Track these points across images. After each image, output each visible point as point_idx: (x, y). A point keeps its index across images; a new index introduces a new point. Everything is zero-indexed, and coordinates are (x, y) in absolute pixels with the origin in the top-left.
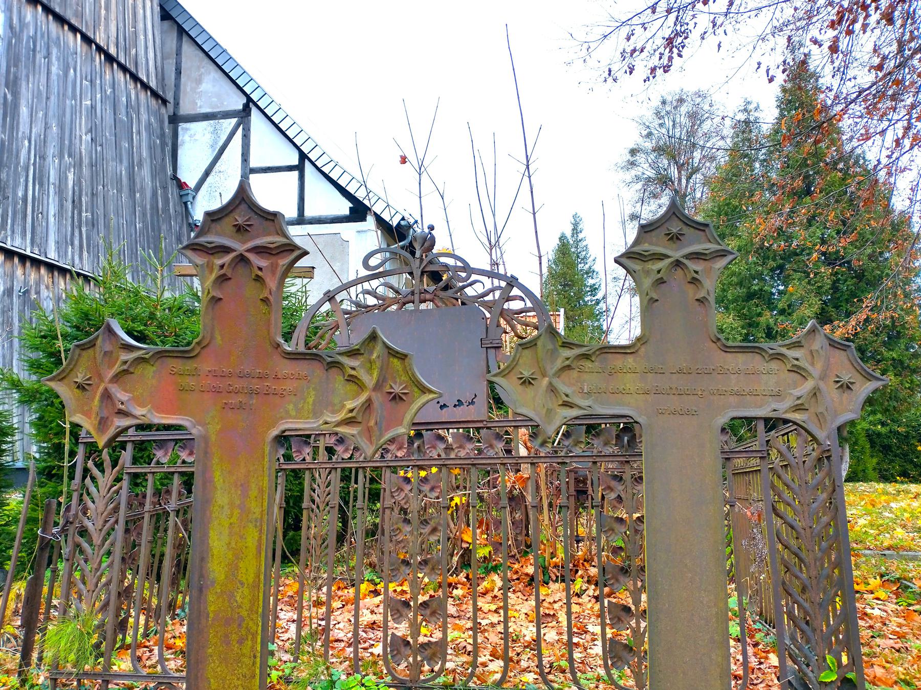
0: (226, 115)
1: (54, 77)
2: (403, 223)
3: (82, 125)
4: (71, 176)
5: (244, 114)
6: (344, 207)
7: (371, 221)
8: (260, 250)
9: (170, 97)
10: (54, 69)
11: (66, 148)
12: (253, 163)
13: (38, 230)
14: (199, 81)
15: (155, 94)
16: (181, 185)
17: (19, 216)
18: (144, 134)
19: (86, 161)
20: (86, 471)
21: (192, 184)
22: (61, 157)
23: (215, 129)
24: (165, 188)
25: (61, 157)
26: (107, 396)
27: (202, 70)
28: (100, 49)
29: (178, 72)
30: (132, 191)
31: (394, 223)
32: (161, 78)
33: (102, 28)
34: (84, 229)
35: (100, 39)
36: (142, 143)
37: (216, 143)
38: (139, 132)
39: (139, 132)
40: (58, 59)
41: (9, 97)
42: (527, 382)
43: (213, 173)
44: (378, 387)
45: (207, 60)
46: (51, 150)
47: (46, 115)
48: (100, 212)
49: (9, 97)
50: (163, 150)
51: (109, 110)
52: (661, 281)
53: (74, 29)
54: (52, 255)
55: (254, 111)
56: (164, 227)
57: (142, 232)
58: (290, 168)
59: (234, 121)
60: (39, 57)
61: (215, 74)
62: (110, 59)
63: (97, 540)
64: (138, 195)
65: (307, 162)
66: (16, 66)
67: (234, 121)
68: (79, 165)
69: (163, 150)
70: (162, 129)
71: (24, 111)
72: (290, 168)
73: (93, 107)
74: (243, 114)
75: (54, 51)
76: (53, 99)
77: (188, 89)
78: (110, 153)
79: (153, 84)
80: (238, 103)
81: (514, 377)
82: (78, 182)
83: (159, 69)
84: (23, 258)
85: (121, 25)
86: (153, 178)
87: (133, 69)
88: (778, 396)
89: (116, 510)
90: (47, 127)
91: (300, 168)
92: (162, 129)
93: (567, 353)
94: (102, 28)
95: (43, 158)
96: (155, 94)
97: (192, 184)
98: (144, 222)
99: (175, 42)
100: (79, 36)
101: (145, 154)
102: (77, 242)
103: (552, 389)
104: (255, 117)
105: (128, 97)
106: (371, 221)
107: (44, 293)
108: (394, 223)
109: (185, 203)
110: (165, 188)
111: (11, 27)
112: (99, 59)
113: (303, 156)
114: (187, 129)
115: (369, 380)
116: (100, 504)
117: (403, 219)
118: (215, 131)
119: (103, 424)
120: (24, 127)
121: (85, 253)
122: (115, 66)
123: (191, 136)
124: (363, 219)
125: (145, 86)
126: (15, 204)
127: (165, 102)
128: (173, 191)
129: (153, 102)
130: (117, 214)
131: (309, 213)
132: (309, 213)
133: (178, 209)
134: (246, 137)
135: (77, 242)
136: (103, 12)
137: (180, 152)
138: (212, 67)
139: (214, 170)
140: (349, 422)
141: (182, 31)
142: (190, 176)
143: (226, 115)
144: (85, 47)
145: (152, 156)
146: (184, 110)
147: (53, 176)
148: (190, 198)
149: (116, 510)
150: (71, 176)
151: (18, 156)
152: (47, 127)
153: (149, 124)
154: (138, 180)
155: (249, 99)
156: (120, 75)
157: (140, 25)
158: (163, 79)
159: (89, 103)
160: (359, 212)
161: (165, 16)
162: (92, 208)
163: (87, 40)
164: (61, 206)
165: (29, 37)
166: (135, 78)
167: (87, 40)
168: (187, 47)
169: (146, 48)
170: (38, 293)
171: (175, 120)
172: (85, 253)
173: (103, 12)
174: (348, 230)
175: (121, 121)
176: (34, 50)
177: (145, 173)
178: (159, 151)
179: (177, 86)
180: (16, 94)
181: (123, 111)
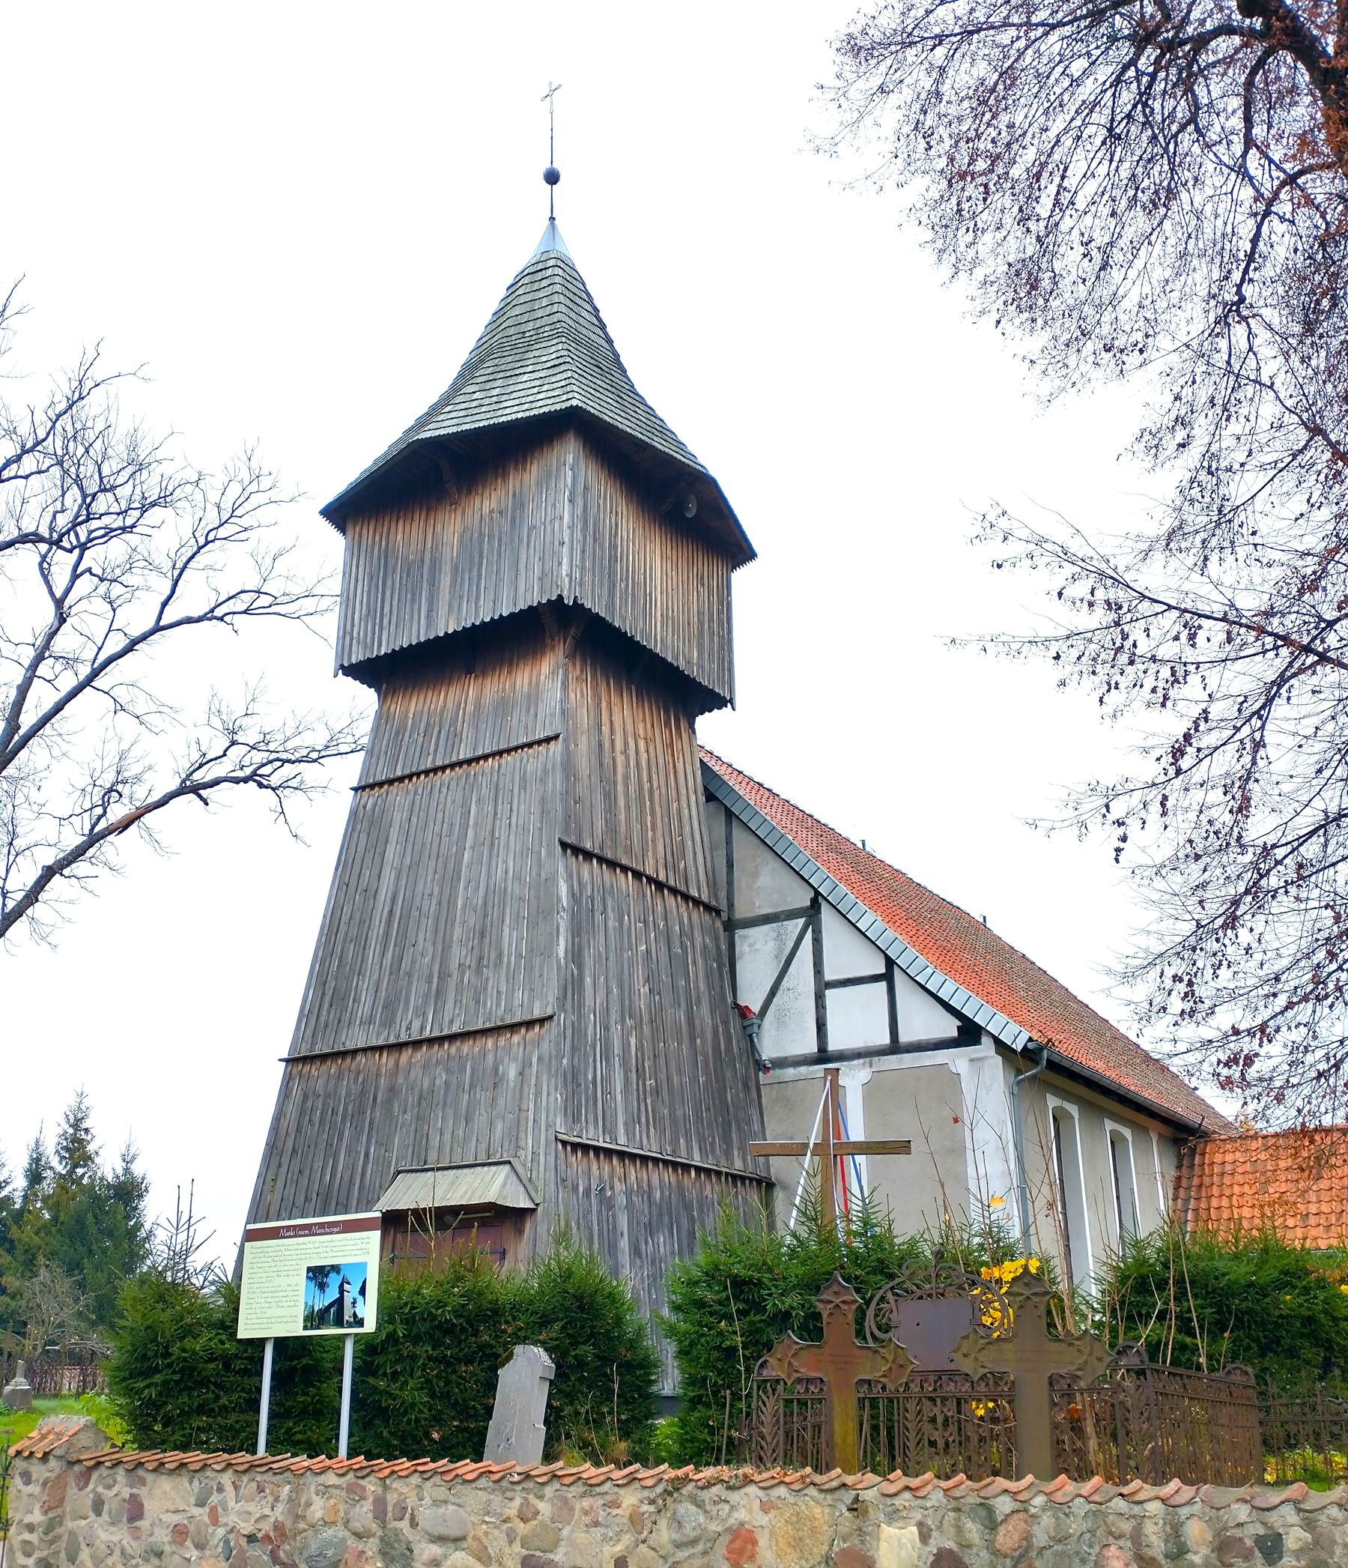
0: (792, 915)
1: (611, 932)
2: (1030, 1045)
3: (640, 974)
4: (633, 1041)
5: (812, 912)
6: (949, 1028)
7: (987, 1047)
8: (843, 1302)
9: (723, 905)
10: (611, 923)
11: (628, 1010)
12: (829, 976)
13: (608, 1112)
14: (755, 875)
15: (708, 908)
16: (743, 1012)
17: (591, 1102)
18: (700, 961)
19: (645, 1018)
20: (759, 1396)
21: (756, 1008)
22: (623, 1021)
23: (779, 935)
24: (726, 1023)
25: (623, 1021)
26: (790, 1363)
27: (759, 860)
28: (650, 879)
29: (730, 865)
30: (692, 1038)
31: (1018, 1046)
32: (713, 885)
33: (650, 854)
34: (649, 1101)
35: (650, 871)
36: (698, 971)
37: (780, 951)
38: (694, 963)
39: (694, 963)
40: (613, 910)
41: (575, 972)
42: (965, 1355)
43: (780, 992)
44: (894, 1361)
45: (762, 847)
46: (614, 1016)
47: (607, 978)
48: (663, 1076)
49: (575, 972)
50: (721, 975)
51: (664, 948)
52: (1021, 1307)
53: (625, 869)
54: (622, 1143)
55: (824, 906)
56: (729, 1074)
57: (706, 1088)
58: (875, 979)
59: (801, 921)
60: (597, 914)
61: (774, 864)
62: (660, 886)
63: (769, 1440)
64: (698, 1041)
65: (896, 970)
66: (579, 935)
67: (801, 921)
68: (639, 1027)
69: (721, 975)
70: (718, 947)
71: (588, 980)
72: (875, 979)
73: (648, 951)
74: (812, 912)
75: (609, 902)
76: (612, 957)
77: (743, 885)
78: (667, 1000)
79: (705, 898)
80: (804, 900)
81: (960, 1353)
82: (640, 1048)
83: (710, 874)
84: (597, 1150)
85: (668, 840)
86: (712, 1013)
87: (683, 889)
88: (1072, 1363)
89: (778, 1421)
90: (608, 992)
91: (888, 977)
92: (718, 947)
93: (983, 1341)
94: (650, 854)
95: (607, 1029)
96: (708, 908)
97: (756, 1008)
98: (707, 1073)
99: (723, 827)
100: (630, 874)
101: (702, 986)
102: (643, 1119)
103: (976, 1359)
104: (826, 915)
105: (681, 924)
106: (987, 1047)
107: (619, 1187)
108: (1018, 1046)
109: (750, 1036)
110: (726, 1023)
111: (573, 895)
112: (649, 890)
113: (890, 963)
114: (745, 937)
115: (890, 1358)
116: (769, 1418)
117: (1030, 1040)
118: (779, 938)
119: (789, 1376)
120: (589, 1001)
121: (652, 1130)
122: (666, 892)
123: (750, 946)
124: (976, 1041)
125: (697, 902)
126: (587, 1088)
127: (718, 912)
128: (734, 1022)
129: (707, 917)
130: (679, 1072)
131: (904, 1038)
132: (904, 1038)
133: (743, 1045)
134: (817, 941)
135: (643, 1119)
136: (650, 834)
137: (738, 966)
138: (769, 855)
139: (781, 988)
140: (884, 1376)
141: (730, 815)
142: (752, 998)
143: (792, 915)
144: (636, 883)
145: (710, 986)
146: (741, 912)
147: (617, 1049)
148: (755, 1027)
149: (778, 1421)
150: (633, 1041)
151: (586, 1035)
152: (608, 992)
153: (705, 947)
154: (697, 1023)
155: (817, 893)
156: (671, 901)
157: (687, 829)
158: (715, 884)
159: (644, 947)
160: (970, 1033)
161: (710, 797)
162: (655, 1075)
163: (638, 875)
164: (627, 1079)
165: (588, 897)
166: (686, 897)
167: (638, 875)
168: (738, 833)
169: (695, 854)
170: (612, 1188)
171: (731, 926)
172: (652, 1130)
173: (650, 834)
174: (958, 1060)
175: (676, 954)
176: (592, 910)
177: (705, 1010)
178: (716, 975)
179: (730, 882)
180: (580, 967)
181: (678, 943)
